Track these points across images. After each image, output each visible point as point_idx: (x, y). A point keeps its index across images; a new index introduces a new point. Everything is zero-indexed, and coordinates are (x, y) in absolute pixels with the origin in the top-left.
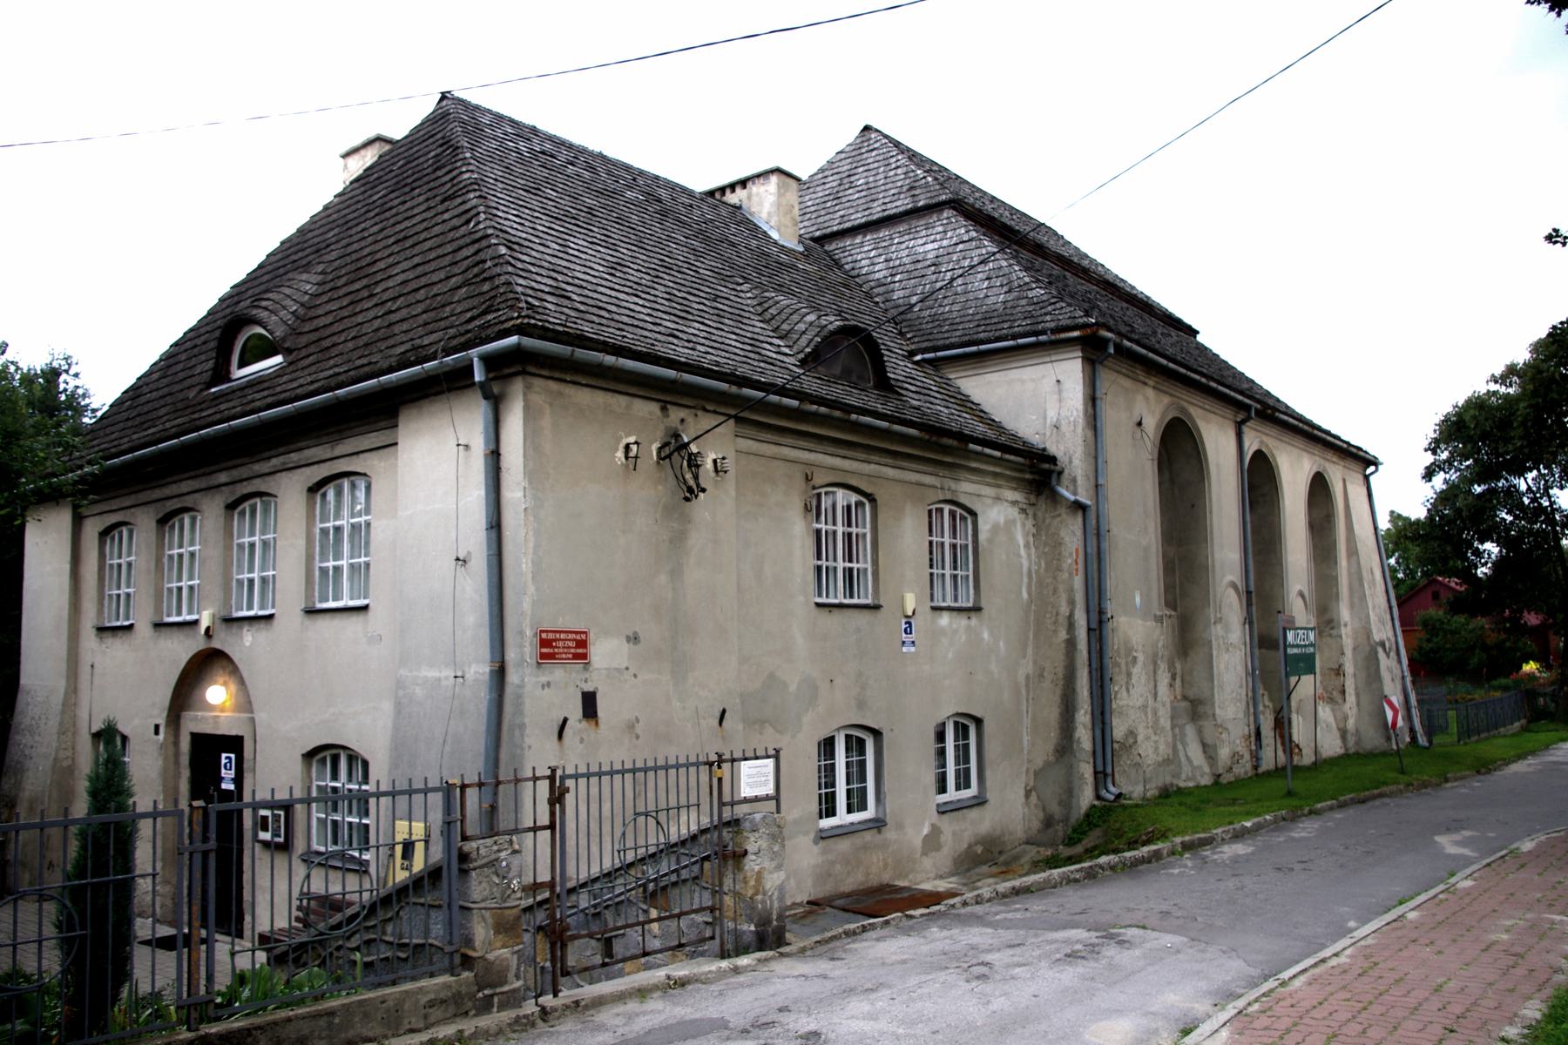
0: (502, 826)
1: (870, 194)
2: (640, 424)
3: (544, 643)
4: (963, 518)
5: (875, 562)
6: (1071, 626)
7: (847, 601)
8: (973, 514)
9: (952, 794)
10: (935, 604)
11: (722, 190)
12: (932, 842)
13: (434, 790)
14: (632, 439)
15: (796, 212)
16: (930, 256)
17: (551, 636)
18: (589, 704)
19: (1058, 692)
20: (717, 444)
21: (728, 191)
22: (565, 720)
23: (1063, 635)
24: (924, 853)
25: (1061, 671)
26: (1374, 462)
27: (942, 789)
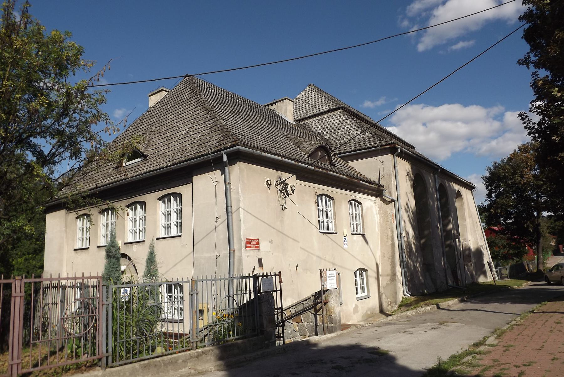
0: (105, 287)
1: (315, 106)
2: (272, 174)
3: (247, 243)
4: (358, 206)
5: (335, 219)
6: (393, 239)
7: (328, 231)
8: (360, 204)
9: (360, 295)
10: (321, 231)
11: (268, 105)
12: (356, 310)
13: (94, 277)
14: (268, 179)
15: (293, 111)
16: (336, 124)
17: (249, 241)
18: (260, 261)
19: (390, 261)
20: (291, 180)
21: (270, 106)
22: (255, 267)
23: (390, 242)
24: (354, 314)
25: (390, 254)
26: (474, 188)
27: (357, 293)
